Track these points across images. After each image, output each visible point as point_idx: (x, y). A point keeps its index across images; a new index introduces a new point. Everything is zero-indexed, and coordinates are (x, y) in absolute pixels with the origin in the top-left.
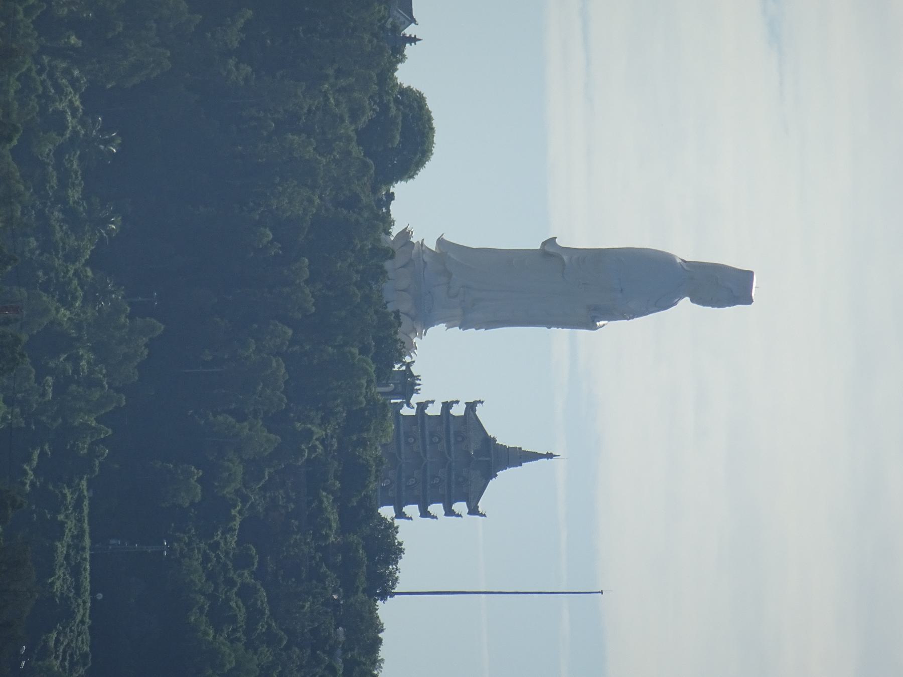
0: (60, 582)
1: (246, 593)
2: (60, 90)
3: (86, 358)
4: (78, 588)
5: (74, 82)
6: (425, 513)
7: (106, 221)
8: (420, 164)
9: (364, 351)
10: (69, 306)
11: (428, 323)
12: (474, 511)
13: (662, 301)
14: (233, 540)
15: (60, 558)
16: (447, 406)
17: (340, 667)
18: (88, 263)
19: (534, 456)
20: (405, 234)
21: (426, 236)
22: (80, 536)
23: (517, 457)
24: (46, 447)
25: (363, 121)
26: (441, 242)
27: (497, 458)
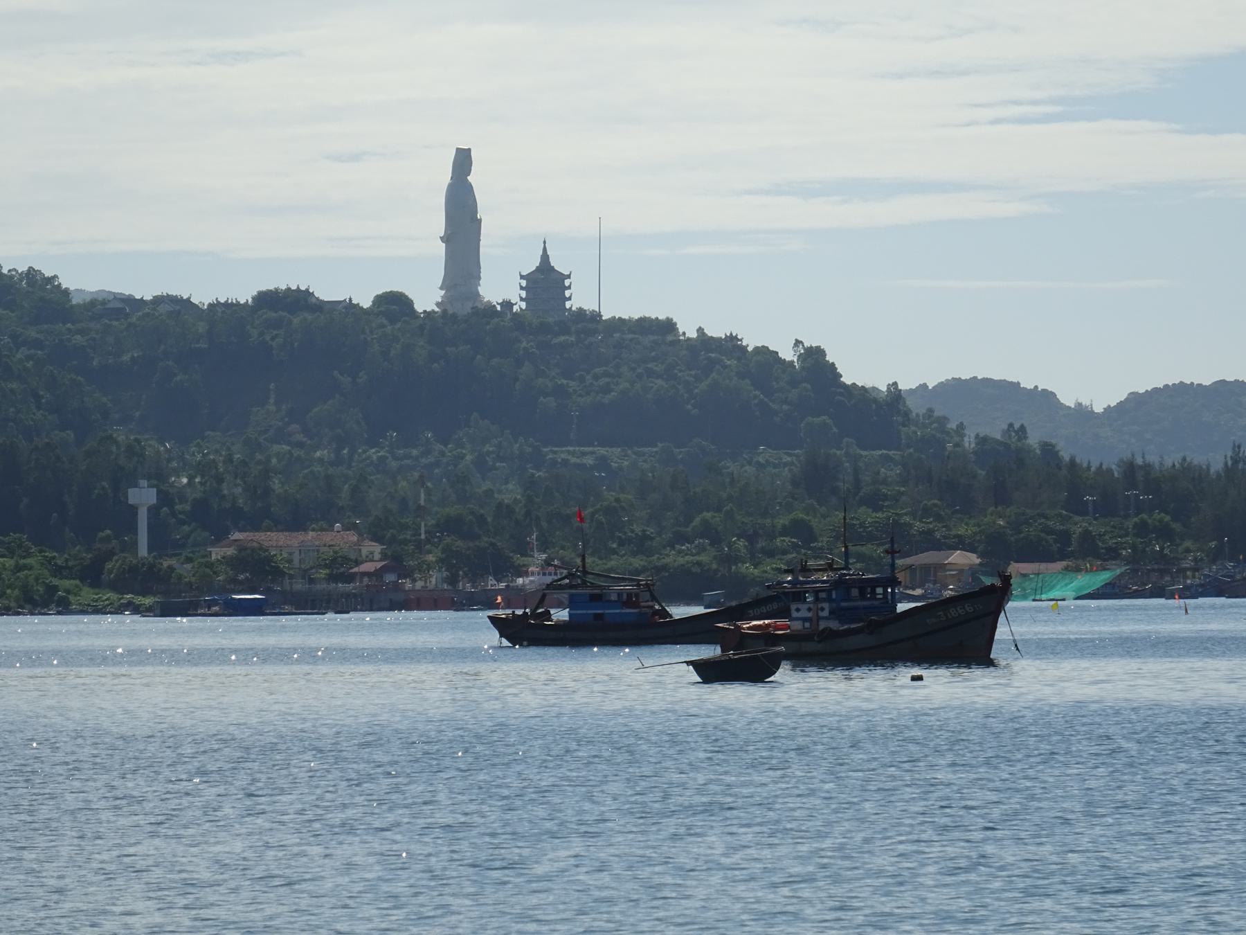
0: (589, 461)
1: (596, 378)
2: (368, 458)
3: (488, 448)
4: (592, 453)
5: (364, 452)
6: (570, 299)
7: (427, 438)
8: (406, 297)
9: (488, 323)
10: (465, 455)
11: (478, 295)
12: (569, 277)
13: (470, 188)
14: (572, 383)
15: (578, 461)
16: (522, 288)
17: (631, 336)
18: (446, 446)
19: (545, 249)
20: (438, 304)
21: (439, 295)
22: (569, 452)
23: (545, 257)
24: (660, 382)
25: (385, 322)
26: (441, 288)
27: (545, 266)
